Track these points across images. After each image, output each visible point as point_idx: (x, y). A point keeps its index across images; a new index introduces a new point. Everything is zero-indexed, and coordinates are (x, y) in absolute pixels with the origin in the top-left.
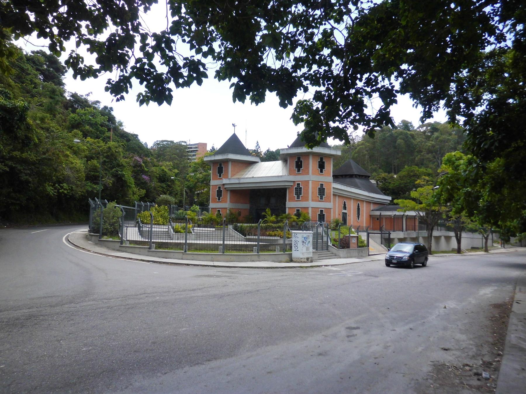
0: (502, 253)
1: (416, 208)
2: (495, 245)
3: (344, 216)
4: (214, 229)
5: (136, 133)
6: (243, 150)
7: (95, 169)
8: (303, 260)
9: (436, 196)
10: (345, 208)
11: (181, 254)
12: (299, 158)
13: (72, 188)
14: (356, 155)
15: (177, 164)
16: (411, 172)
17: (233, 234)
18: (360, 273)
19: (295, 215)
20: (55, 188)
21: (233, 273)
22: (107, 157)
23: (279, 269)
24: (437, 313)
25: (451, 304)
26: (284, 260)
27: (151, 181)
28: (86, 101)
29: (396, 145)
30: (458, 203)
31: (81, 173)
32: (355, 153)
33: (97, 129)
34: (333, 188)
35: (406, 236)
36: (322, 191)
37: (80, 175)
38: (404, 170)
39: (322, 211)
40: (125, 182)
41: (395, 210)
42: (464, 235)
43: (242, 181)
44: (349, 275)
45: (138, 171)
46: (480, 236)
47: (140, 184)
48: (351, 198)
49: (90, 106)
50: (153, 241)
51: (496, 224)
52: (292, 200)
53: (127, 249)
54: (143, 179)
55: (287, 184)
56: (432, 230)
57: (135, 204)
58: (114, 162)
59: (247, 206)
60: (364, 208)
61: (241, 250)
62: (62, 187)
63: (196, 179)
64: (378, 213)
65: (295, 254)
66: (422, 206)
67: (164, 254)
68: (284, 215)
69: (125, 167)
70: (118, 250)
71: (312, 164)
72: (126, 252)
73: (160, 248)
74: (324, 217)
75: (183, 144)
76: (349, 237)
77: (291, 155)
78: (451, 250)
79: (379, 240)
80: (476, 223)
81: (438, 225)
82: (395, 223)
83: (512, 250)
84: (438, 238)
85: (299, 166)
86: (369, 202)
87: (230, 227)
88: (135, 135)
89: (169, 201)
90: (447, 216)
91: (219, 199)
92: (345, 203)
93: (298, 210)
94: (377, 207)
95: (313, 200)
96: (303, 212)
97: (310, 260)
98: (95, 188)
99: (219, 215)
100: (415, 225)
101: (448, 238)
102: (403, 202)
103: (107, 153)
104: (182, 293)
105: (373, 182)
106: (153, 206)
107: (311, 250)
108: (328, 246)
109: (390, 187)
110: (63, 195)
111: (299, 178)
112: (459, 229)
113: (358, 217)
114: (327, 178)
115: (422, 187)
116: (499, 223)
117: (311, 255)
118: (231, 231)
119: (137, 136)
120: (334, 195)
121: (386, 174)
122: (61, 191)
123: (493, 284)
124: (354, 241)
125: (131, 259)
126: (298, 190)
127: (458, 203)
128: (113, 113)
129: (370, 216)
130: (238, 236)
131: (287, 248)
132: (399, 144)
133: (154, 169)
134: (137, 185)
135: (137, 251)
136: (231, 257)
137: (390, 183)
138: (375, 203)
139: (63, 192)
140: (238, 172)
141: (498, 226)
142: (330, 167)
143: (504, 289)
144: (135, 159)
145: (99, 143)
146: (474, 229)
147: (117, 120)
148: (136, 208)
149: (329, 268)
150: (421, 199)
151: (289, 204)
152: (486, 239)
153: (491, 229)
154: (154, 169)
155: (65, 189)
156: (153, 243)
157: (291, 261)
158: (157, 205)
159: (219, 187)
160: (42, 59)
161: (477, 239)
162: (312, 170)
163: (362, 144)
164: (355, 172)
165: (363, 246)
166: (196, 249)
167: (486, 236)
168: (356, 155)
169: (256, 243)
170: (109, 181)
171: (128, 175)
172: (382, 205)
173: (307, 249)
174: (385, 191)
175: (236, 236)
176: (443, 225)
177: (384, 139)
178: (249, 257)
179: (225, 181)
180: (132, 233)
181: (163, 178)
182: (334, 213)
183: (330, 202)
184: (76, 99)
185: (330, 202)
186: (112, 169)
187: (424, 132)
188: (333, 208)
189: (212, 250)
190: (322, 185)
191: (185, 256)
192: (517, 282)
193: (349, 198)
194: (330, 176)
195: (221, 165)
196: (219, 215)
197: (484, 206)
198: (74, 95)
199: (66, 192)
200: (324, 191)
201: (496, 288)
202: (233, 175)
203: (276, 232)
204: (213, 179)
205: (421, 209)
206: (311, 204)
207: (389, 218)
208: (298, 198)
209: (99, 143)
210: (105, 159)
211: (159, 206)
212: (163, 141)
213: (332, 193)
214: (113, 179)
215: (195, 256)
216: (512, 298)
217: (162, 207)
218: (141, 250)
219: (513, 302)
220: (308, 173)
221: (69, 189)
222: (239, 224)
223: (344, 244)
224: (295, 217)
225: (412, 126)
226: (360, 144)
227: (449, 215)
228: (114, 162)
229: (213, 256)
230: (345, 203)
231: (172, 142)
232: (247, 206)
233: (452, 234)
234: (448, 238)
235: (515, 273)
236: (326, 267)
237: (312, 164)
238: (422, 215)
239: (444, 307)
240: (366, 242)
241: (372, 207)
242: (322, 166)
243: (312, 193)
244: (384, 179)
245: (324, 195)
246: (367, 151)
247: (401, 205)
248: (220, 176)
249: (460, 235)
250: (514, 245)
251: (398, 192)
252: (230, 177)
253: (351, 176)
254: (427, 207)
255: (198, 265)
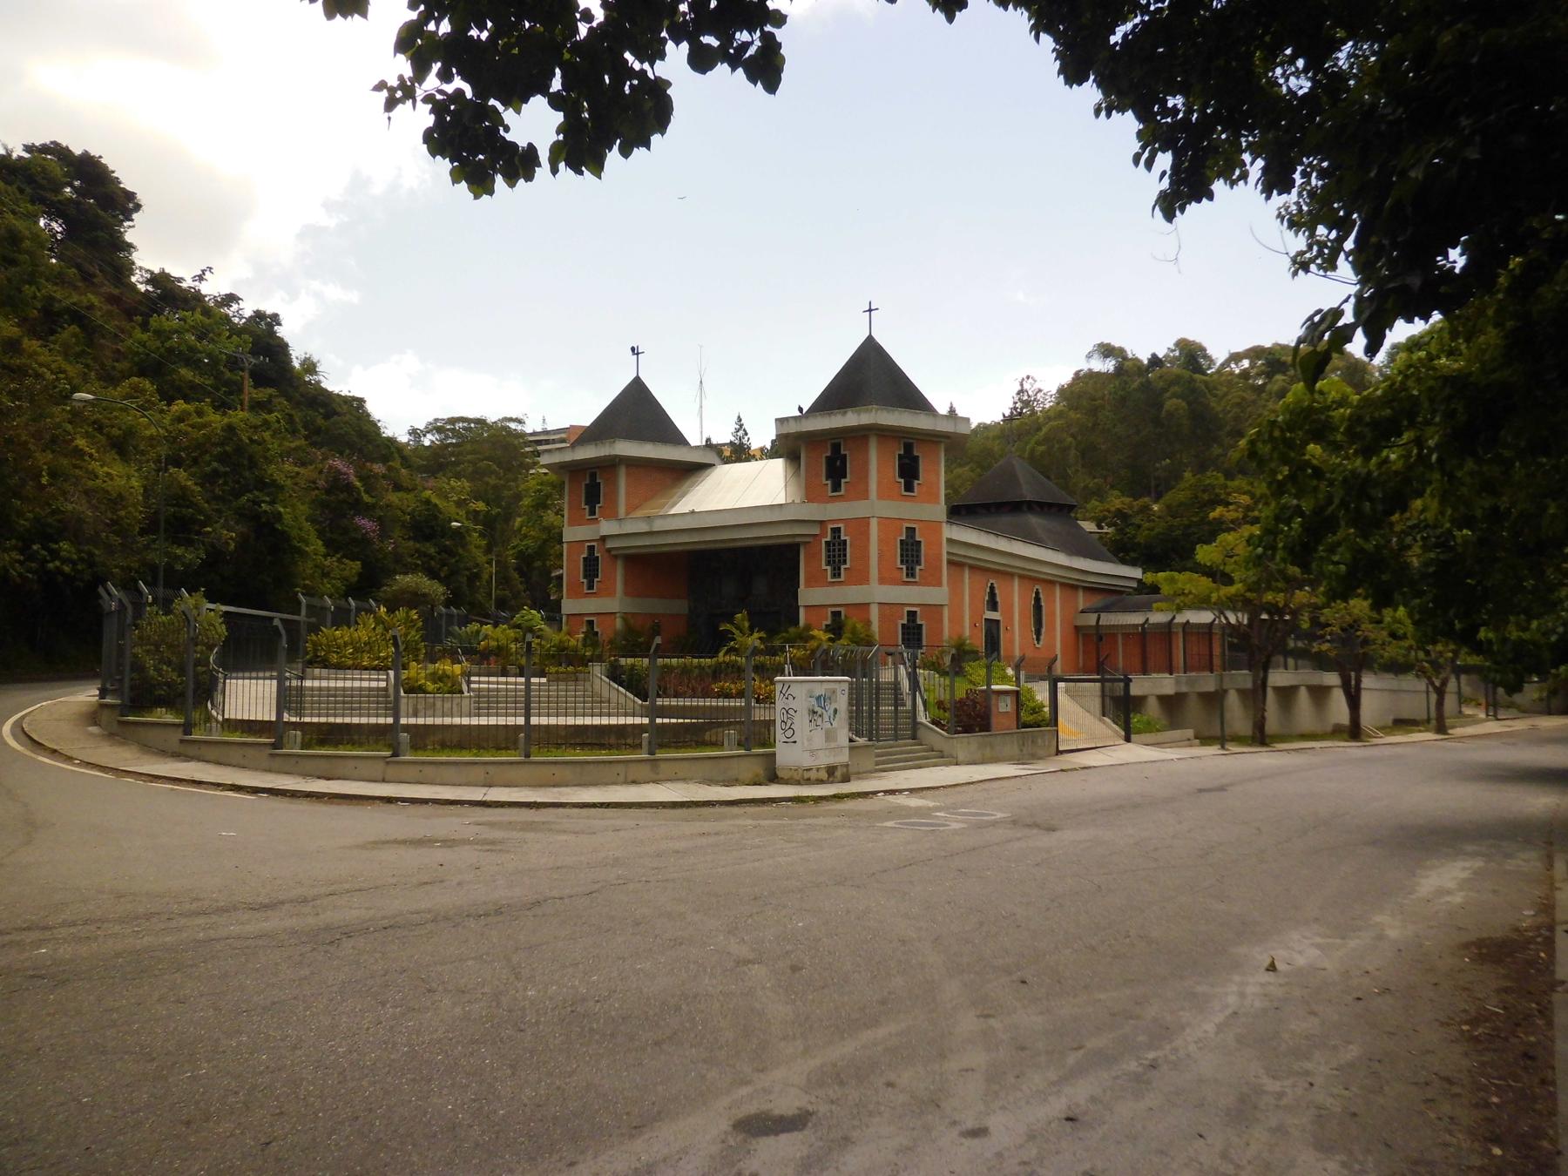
0: (1495, 736)
1: (1214, 597)
2: (1467, 711)
3: (993, 629)
4: (544, 680)
5: (358, 395)
6: (666, 431)
7: (181, 497)
8: (813, 775)
9: (1260, 538)
10: (993, 605)
11: (380, 765)
12: (836, 448)
13: (91, 554)
14: (1042, 448)
15: (495, 487)
16: (1204, 491)
17: (605, 694)
18: (999, 815)
19: (828, 629)
20: (31, 557)
21: (510, 825)
22: (223, 458)
23: (718, 810)
24: (1232, 1000)
25: (1302, 950)
26: (748, 776)
27: (384, 534)
28: (198, 297)
29: (1163, 414)
30: (1336, 558)
31: (124, 507)
32: (1038, 443)
33: (218, 377)
34: (950, 541)
35: (1184, 689)
36: (910, 551)
37: (122, 513)
38: (1182, 485)
39: (912, 615)
40: (284, 537)
41: (1147, 607)
42: (1368, 681)
43: (659, 526)
44: (955, 826)
45: (338, 506)
46: (1422, 685)
47: (340, 541)
48: (1012, 575)
49: (207, 312)
50: (403, 721)
51: (1467, 639)
52: (815, 581)
53: (212, 753)
54: (358, 528)
55: (798, 530)
56: (1266, 669)
57: (299, 603)
58: (247, 474)
59: (680, 606)
60: (1057, 608)
61: (602, 746)
62: (55, 554)
63: (545, 529)
64: (1091, 620)
65: (786, 755)
66: (1232, 590)
67: (323, 765)
68: (792, 630)
69: (282, 488)
70: (177, 756)
71: (878, 465)
72: (199, 759)
73: (322, 743)
74: (920, 634)
75: (513, 426)
76: (989, 693)
77: (812, 440)
78: (1329, 729)
79: (1096, 704)
80: (1406, 643)
81: (1288, 653)
82: (1153, 648)
83: (1521, 725)
84: (1287, 695)
85: (836, 471)
86: (1071, 587)
87: (597, 670)
88: (354, 399)
89: (424, 595)
90: (1315, 621)
91: (591, 587)
92: (992, 588)
93: (836, 615)
94: (1098, 601)
95: (882, 581)
96: (852, 621)
97: (838, 774)
98: (178, 558)
99: (591, 635)
100: (1211, 656)
101: (1319, 694)
102: (1172, 581)
103: (222, 444)
104: (215, 918)
105: (1089, 526)
106: (370, 611)
107: (843, 735)
108: (915, 725)
109: (1140, 539)
110: (60, 579)
111: (837, 511)
112: (1353, 660)
113: (1038, 633)
114: (927, 509)
115: (1229, 530)
116: (1483, 634)
117: (844, 757)
118: (597, 681)
119: (361, 401)
120: (950, 562)
121: (1127, 500)
122: (51, 565)
123: (1469, 848)
124: (1005, 706)
125: (199, 783)
126: (837, 552)
127: (1336, 558)
128: (281, 331)
129: (1077, 629)
130: (622, 700)
131: (759, 736)
132: (1170, 414)
133: (394, 498)
134: (332, 546)
135: (449, 773)
136: (553, 769)
137: (1139, 526)
138: (1091, 590)
139: (59, 571)
140: (646, 499)
141: (1479, 648)
142: (938, 475)
143: (1510, 865)
144: (331, 467)
145: (200, 413)
146: (1401, 660)
147: (297, 355)
148: (302, 617)
149: (900, 800)
150: (1228, 569)
151: (809, 595)
152: (1441, 692)
153: (1453, 660)
154: (394, 498)
155: (64, 561)
156: (407, 728)
157: (773, 778)
158: (383, 609)
159: (591, 548)
160: (58, 171)
161: (1412, 693)
162: (879, 483)
163: (1060, 415)
164: (1028, 495)
165: (1036, 728)
166: (444, 746)
167: (1437, 683)
168: (1042, 448)
169: (646, 721)
170: (227, 534)
171: (296, 515)
172: (1112, 596)
173: (830, 736)
174: (1121, 551)
175: (614, 695)
176: (1300, 654)
177: (1123, 400)
178: (620, 768)
179: (607, 527)
180: (249, 697)
181: (427, 527)
182: (956, 619)
183: (939, 584)
184: (164, 289)
185: (939, 584)
186: (237, 496)
187: (1245, 374)
188: (952, 606)
189: (498, 749)
190: (911, 531)
191: (391, 771)
192: (1556, 837)
193: (1006, 574)
194: (937, 501)
195: (593, 476)
196: (591, 635)
197: (1426, 564)
198: (160, 280)
199: (66, 569)
200: (919, 551)
201: (1478, 863)
202: (632, 508)
203: (742, 685)
204: (571, 524)
205: (1233, 603)
206: (879, 593)
207: (1129, 633)
208: (836, 574)
209: (200, 413)
210: (215, 464)
211: (391, 610)
212: (453, 421)
213: (945, 557)
214: (239, 528)
215: (428, 770)
216: (1547, 907)
217: (401, 613)
218: (250, 752)
219: (1551, 928)
220: (865, 495)
221: (82, 560)
222: (623, 661)
223: (970, 718)
224: (824, 636)
225: (1207, 357)
226: (1052, 414)
227: (1322, 619)
228: (247, 474)
229: (491, 769)
230: (992, 588)
231: (481, 422)
232: (680, 606)
233: (1332, 679)
234: (1319, 694)
235: (1540, 802)
236: (890, 798)
237: (878, 465)
238: (1233, 620)
239: (1267, 962)
240: (1046, 709)
241: (1081, 601)
242: (909, 471)
243: (880, 556)
244: (1120, 514)
245: (918, 563)
246: (1073, 436)
247: (1166, 589)
248: (592, 512)
249: (1358, 682)
250: (1526, 711)
251: (1166, 552)
252: (622, 510)
253: (1016, 507)
254: (1248, 595)
255: (425, 801)
